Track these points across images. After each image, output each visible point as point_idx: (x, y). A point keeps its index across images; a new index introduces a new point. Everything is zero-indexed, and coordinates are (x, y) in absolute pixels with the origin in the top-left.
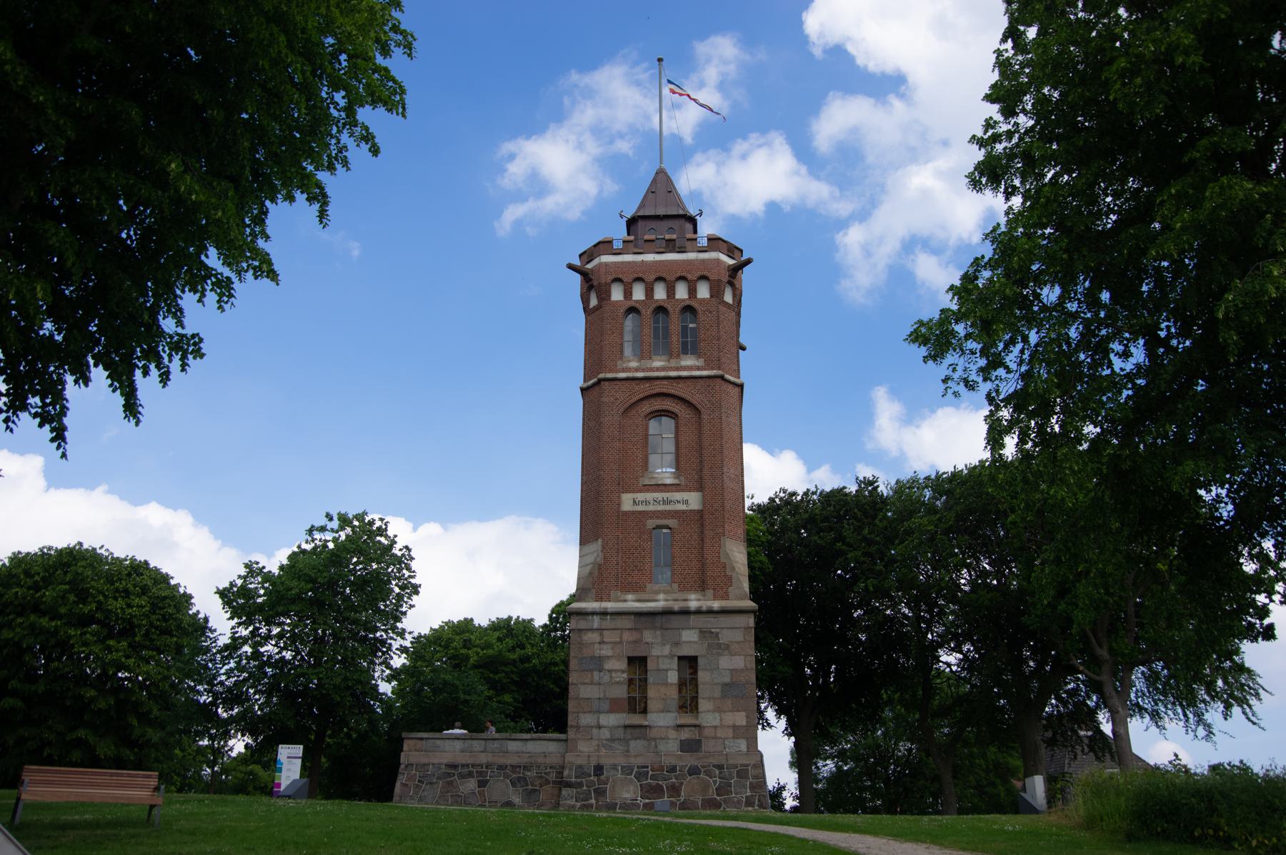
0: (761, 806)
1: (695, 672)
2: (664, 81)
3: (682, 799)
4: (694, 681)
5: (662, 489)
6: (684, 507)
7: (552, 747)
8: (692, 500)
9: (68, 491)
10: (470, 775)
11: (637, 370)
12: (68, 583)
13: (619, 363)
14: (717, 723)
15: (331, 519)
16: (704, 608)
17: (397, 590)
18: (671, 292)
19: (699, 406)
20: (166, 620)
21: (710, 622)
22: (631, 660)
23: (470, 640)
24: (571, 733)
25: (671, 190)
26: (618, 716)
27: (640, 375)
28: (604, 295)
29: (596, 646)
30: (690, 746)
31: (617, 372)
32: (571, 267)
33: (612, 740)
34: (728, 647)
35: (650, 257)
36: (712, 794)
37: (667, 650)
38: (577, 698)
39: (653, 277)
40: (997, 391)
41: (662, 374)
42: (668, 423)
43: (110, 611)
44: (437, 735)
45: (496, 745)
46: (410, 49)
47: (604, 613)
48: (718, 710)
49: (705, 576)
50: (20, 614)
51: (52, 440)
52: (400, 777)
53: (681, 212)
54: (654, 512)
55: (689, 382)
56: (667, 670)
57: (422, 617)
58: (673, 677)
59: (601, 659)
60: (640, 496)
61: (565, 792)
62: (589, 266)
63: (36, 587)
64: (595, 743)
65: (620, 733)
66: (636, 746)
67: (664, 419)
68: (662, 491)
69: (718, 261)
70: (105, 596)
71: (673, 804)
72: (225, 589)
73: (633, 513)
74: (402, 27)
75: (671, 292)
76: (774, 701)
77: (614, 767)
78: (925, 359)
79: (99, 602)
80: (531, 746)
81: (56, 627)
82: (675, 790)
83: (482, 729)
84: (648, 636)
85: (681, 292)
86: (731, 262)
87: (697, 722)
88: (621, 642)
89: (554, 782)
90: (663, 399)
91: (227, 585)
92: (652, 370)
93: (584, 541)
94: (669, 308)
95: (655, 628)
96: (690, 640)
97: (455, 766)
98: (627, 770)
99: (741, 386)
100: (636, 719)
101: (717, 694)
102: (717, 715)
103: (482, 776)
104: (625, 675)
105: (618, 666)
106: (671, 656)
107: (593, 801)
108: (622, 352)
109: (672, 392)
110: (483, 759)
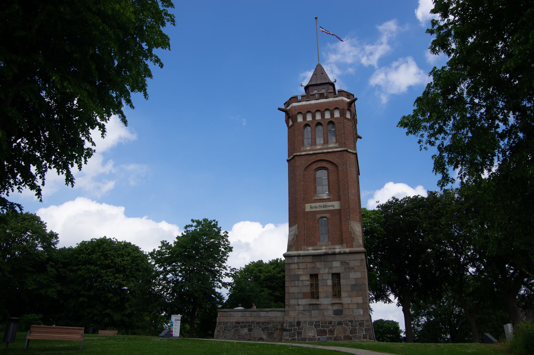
0: (370, 339)
1: (340, 280)
2: (318, 26)
3: (335, 336)
4: (339, 284)
5: (323, 202)
6: (332, 208)
7: (279, 314)
8: (336, 205)
9: (136, 219)
10: (245, 326)
11: (310, 150)
12: (101, 252)
13: (302, 148)
14: (349, 302)
15: (194, 222)
16: (342, 252)
17: (223, 249)
18: (323, 116)
19: (337, 164)
20: (138, 266)
21: (346, 258)
22: (312, 276)
23: (261, 269)
24: (287, 308)
25: (323, 73)
26: (306, 300)
27: (311, 152)
28: (295, 120)
29: (296, 270)
30: (338, 313)
31: (301, 152)
32: (280, 109)
33: (304, 310)
34: (353, 268)
35: (313, 102)
36: (348, 333)
37: (326, 271)
38: (289, 293)
39: (315, 110)
40: (443, 145)
41: (321, 151)
42: (325, 172)
43: (116, 263)
44: (231, 310)
45: (255, 313)
46: (174, 22)
47: (299, 256)
48: (350, 296)
49: (343, 237)
50: (84, 265)
51: (36, 195)
52: (217, 328)
53: (327, 81)
54: (319, 211)
55: (332, 154)
56: (327, 280)
57: (237, 261)
58: (330, 282)
59: (298, 276)
60: (313, 205)
61: (285, 333)
62: (288, 108)
63: (89, 254)
64: (297, 312)
65: (307, 307)
66: (315, 313)
67: (323, 170)
68: (322, 202)
69: (343, 100)
70: (114, 257)
71: (331, 338)
72: (152, 252)
73: (311, 212)
74: (168, 13)
75: (323, 116)
76: (393, 291)
77: (305, 322)
78: (407, 134)
79: (112, 259)
80: (270, 314)
81: (97, 269)
82: (332, 332)
83: (251, 307)
84: (318, 265)
85: (327, 116)
86: (348, 100)
87: (341, 302)
88: (307, 268)
89: (280, 329)
90: (321, 161)
91: (152, 251)
92: (316, 150)
93: (290, 226)
94: (322, 123)
95: (321, 261)
96: (337, 266)
97: (238, 323)
98: (311, 323)
99: (356, 154)
100: (314, 301)
101: (349, 289)
102: (349, 299)
103: (250, 326)
104: (309, 282)
105: (305, 278)
106: (329, 273)
107: (296, 337)
108: (303, 143)
109: (325, 159)
110: (250, 320)
